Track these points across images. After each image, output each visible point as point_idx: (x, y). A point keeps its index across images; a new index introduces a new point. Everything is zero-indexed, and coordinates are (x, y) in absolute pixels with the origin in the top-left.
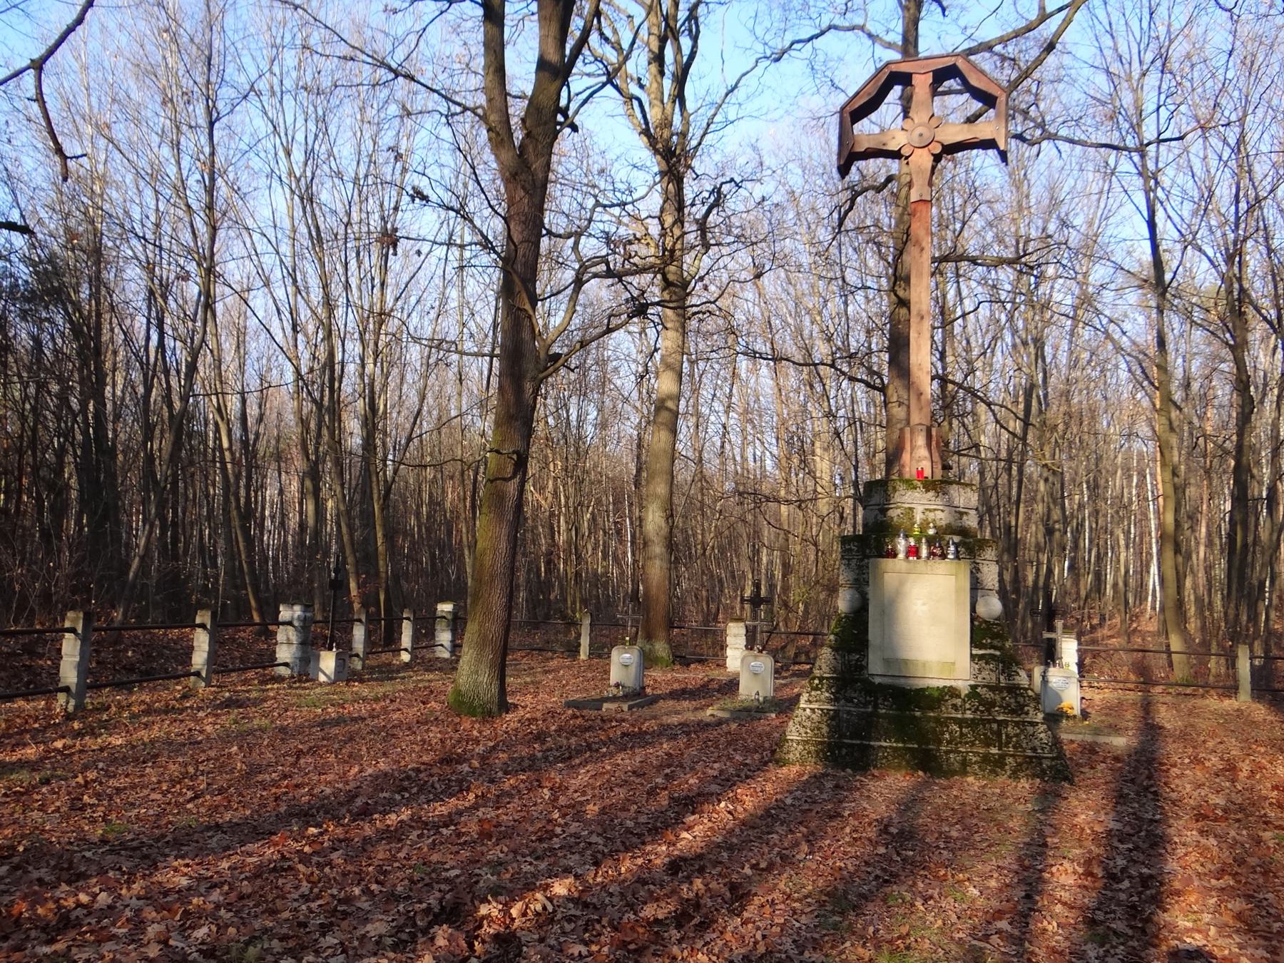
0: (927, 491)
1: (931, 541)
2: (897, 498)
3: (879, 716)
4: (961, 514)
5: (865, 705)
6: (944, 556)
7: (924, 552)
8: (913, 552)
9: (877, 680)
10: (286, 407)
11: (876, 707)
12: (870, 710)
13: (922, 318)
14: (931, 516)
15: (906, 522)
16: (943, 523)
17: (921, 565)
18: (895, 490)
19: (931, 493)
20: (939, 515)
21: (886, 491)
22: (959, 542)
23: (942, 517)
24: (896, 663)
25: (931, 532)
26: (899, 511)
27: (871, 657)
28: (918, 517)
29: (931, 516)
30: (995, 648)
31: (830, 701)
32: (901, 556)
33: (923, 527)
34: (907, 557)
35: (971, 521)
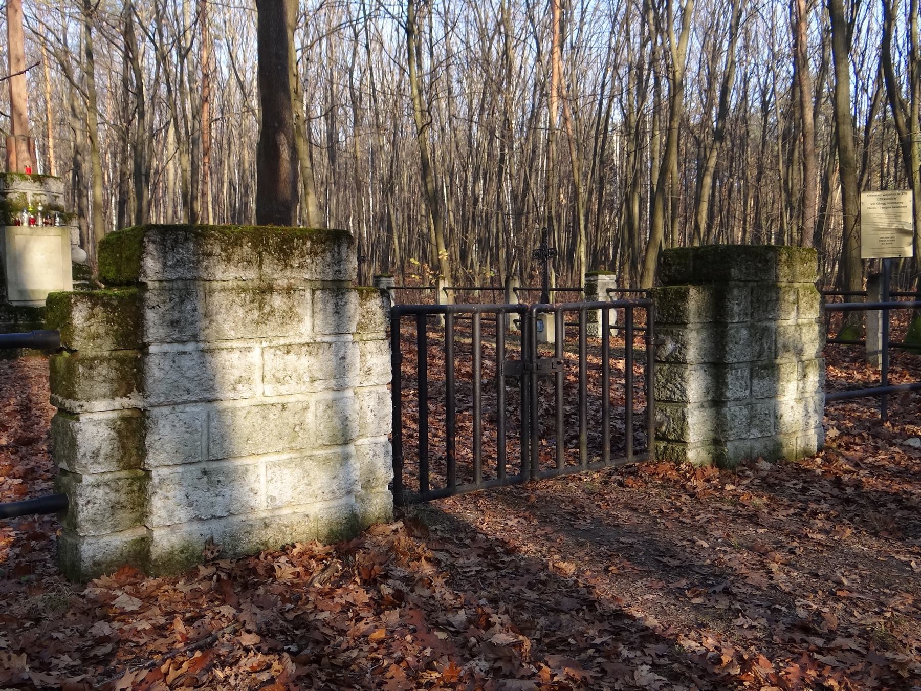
0: (35, 182)
1: (44, 214)
2: (15, 185)
3: (19, 326)
4: (56, 197)
5: (9, 320)
6: (52, 224)
7: (40, 222)
8: (32, 222)
9: (15, 304)
10: (267, 261)
11: (16, 320)
12: (12, 322)
13: (19, 60)
14: (38, 198)
15: (22, 203)
16: (47, 203)
17: (40, 230)
18: (12, 180)
19: (37, 184)
20: (44, 197)
21: (5, 181)
22: (50, 214)
23: (45, 199)
24: (22, 292)
25: (40, 208)
26: (16, 195)
27: (9, 289)
28: (30, 199)
29: (38, 198)
30: (86, 279)
31: (779, 326)
32: (26, 224)
33: (35, 204)
34: (29, 224)
35: (61, 202)
